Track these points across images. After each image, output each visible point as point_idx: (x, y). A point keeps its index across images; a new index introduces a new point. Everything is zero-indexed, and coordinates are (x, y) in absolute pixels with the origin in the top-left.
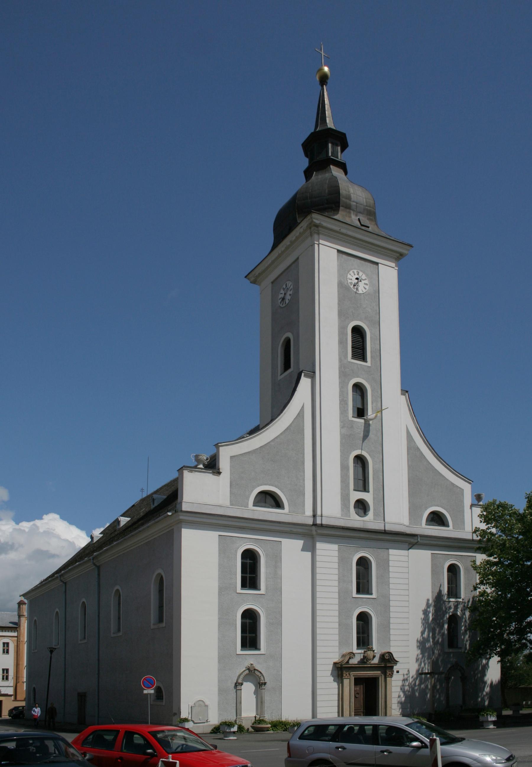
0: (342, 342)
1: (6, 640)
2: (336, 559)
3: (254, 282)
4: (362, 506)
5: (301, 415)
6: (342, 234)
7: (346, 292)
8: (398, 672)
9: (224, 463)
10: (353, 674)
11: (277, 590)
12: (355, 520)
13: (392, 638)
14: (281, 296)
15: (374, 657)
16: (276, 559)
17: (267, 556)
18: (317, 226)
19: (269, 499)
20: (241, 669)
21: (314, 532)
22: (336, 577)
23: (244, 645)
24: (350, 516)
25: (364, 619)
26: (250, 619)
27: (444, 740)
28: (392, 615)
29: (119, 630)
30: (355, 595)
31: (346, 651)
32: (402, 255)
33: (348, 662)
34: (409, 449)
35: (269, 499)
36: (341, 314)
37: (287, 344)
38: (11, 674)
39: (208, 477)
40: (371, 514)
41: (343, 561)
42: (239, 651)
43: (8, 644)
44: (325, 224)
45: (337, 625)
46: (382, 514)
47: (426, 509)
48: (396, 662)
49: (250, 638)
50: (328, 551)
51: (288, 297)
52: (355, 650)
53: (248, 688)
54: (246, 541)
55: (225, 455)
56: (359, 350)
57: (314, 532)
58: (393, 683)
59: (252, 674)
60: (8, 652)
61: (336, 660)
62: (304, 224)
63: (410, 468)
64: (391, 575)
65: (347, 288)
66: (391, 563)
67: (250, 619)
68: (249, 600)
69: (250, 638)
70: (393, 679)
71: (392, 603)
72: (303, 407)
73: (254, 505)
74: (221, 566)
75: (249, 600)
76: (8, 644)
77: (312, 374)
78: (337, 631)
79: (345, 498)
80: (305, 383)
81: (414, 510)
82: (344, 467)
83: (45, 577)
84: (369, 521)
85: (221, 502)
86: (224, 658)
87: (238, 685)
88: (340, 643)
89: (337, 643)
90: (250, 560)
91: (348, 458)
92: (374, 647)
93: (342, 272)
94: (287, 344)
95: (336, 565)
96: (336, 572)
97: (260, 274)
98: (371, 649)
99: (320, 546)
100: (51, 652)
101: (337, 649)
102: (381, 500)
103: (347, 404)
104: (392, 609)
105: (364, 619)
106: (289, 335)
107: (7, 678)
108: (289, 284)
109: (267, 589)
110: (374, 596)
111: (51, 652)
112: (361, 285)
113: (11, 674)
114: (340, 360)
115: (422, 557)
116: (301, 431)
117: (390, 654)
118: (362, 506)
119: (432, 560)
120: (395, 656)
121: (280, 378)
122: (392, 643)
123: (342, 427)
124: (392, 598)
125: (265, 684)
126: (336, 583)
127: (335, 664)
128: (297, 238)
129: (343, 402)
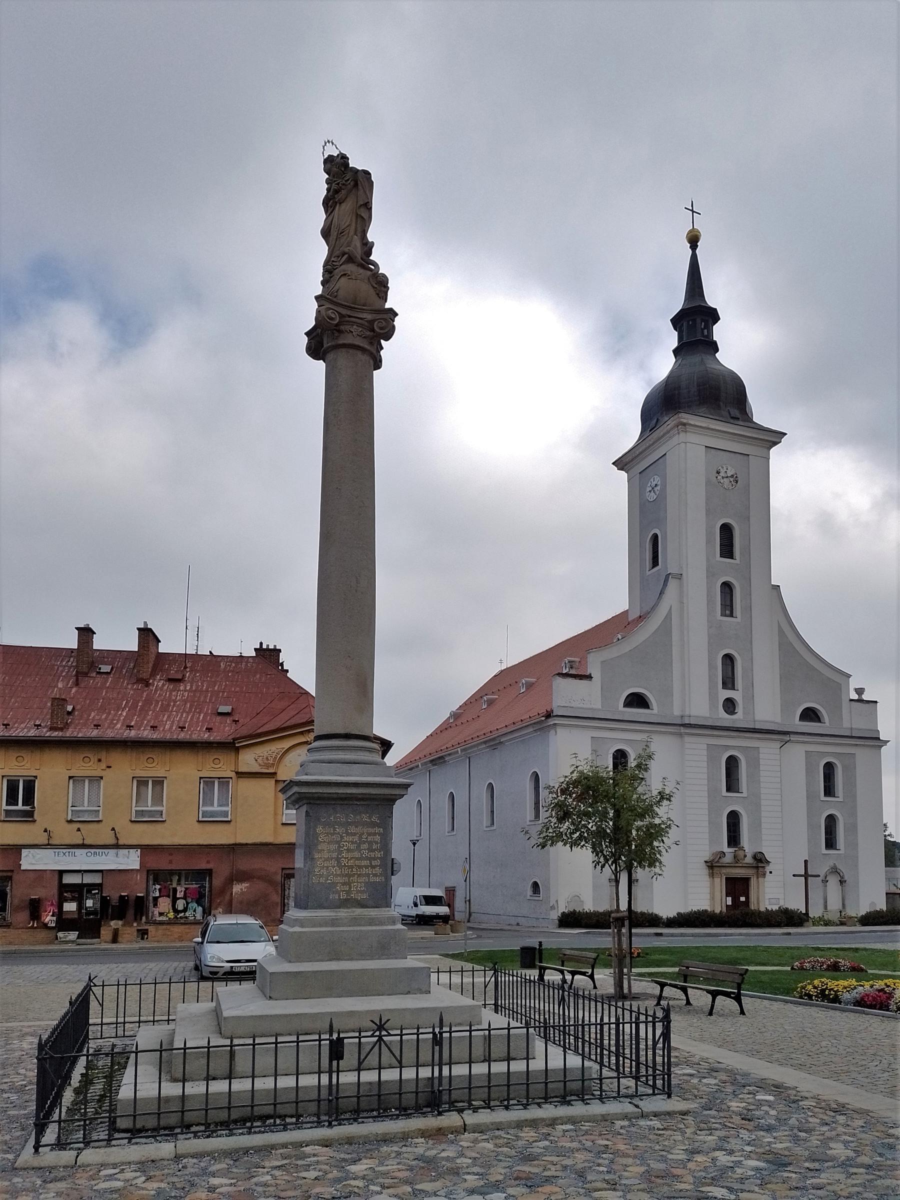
0: (709, 541)
2: (705, 758)
4: (730, 705)
5: (669, 616)
6: (712, 429)
8: (771, 872)
10: (724, 871)
12: (724, 718)
13: (764, 837)
15: (745, 856)
16: (755, 764)
18: (684, 424)
19: (637, 701)
22: (706, 776)
25: (734, 819)
26: (732, 784)
27: (90, 634)
28: (763, 814)
29: (493, 824)
33: (718, 862)
35: (637, 701)
36: (708, 512)
40: (740, 709)
41: (712, 760)
44: (692, 423)
47: (800, 705)
48: (768, 862)
50: (697, 748)
52: (726, 849)
54: (619, 739)
55: (593, 668)
58: (766, 884)
61: (707, 859)
66: (761, 762)
67: (732, 784)
71: (763, 803)
72: (695, 323)
77: (679, 577)
79: (713, 696)
81: (786, 707)
82: (712, 667)
84: (739, 718)
89: (707, 842)
92: (746, 848)
94: (655, 538)
95: (705, 764)
96: (705, 770)
98: (742, 849)
99: (687, 739)
100: (414, 844)
101: (707, 848)
102: (750, 698)
104: (763, 808)
105: (734, 819)
106: (657, 531)
110: (745, 795)
111: (414, 844)
114: (708, 560)
115: (797, 753)
118: (730, 705)
119: (806, 758)
121: (648, 573)
123: (710, 627)
125: (637, 880)
126: (706, 782)
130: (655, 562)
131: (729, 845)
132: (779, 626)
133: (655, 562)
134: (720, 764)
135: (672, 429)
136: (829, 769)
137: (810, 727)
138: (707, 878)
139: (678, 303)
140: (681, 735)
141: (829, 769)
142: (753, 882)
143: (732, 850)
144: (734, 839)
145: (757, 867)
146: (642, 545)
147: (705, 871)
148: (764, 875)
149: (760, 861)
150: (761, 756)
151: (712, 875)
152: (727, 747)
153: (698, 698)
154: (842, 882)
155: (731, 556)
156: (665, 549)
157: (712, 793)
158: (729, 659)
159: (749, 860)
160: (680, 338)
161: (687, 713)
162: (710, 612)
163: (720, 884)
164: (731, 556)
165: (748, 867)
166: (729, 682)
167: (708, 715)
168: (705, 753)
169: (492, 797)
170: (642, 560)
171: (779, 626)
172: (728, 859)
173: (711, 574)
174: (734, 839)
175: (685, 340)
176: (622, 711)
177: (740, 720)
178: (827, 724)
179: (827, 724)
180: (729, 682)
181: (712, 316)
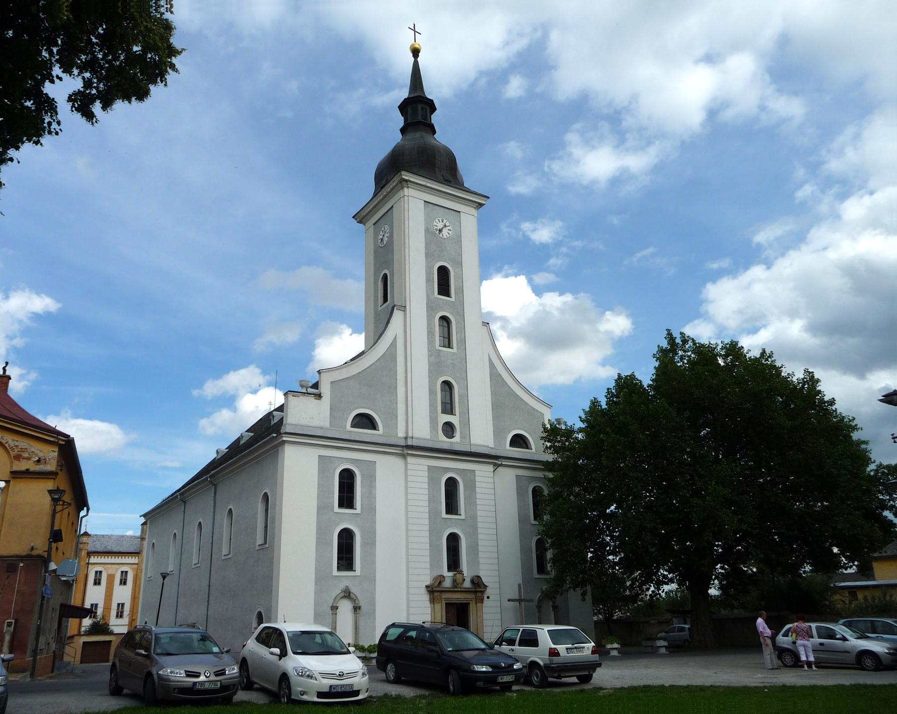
0: (429, 280)
1: (125, 568)
2: (426, 480)
3: (360, 222)
4: (449, 429)
7: (432, 236)
8: (488, 598)
9: (325, 389)
10: (445, 596)
11: (371, 509)
12: (443, 441)
14: (381, 237)
16: (371, 479)
17: (362, 476)
18: (407, 181)
19: (365, 421)
20: (338, 590)
21: (408, 449)
23: (341, 505)
24: (430, 468)
25: (453, 540)
26: (346, 539)
30: (444, 515)
31: (437, 573)
32: (481, 205)
34: (491, 375)
36: (428, 255)
37: (385, 277)
38: (127, 609)
39: (311, 400)
40: (458, 434)
41: (432, 481)
42: (335, 572)
43: (126, 572)
45: (428, 546)
46: (466, 435)
49: (346, 558)
50: (420, 466)
51: (386, 239)
53: (345, 607)
54: (346, 458)
56: (444, 287)
57: (408, 449)
58: (485, 610)
59: (347, 594)
60: (125, 583)
61: (428, 583)
62: (396, 180)
63: (494, 393)
64: (478, 496)
65: (433, 234)
67: (346, 539)
68: (345, 519)
69: (346, 558)
70: (484, 604)
73: (353, 426)
74: (320, 485)
75: (345, 519)
76: (126, 572)
77: (403, 308)
78: (428, 553)
79: (433, 420)
80: (397, 315)
81: (498, 432)
82: (432, 392)
83: (167, 496)
85: (321, 424)
86: (321, 579)
87: (334, 608)
88: (431, 565)
90: (347, 481)
91: (436, 384)
93: (429, 220)
94: (385, 277)
95: (426, 486)
96: (426, 492)
97: (364, 217)
98: (461, 572)
99: (410, 460)
100: (164, 577)
101: (428, 572)
102: (466, 423)
103: (434, 335)
105: (453, 540)
107: (121, 616)
108: (387, 227)
109: (362, 509)
110: (463, 517)
111: (164, 577)
112: (445, 231)
113: (127, 609)
114: (428, 297)
116: (394, 359)
117: (478, 577)
118: (449, 429)
120: (485, 580)
121: (380, 309)
122: (481, 567)
123: (430, 356)
124: (479, 519)
126: (427, 504)
127: (427, 587)
128: (392, 190)
129: (430, 333)
130: (385, 299)
131: (449, 569)
132: (490, 360)
133: (385, 299)
134: (334, 477)
135: (397, 185)
136: (451, 484)
137: (517, 452)
138: (428, 604)
139: (404, 94)
140: (404, 456)
141: (451, 484)
142: (472, 607)
143: (451, 574)
144: (454, 563)
145: (476, 592)
146: (376, 284)
147: (426, 597)
148: (482, 601)
149: (478, 585)
150: (477, 479)
151: (433, 601)
152: (447, 470)
153: (418, 419)
154: (356, 609)
155: (448, 294)
156: (393, 287)
157: (322, 509)
158: (447, 385)
159: (467, 584)
160: (405, 120)
161: (410, 435)
162: (431, 341)
163: (440, 608)
164: (448, 294)
165: (467, 591)
166: (448, 408)
167: (428, 437)
168: (426, 474)
169: (267, 510)
170: (376, 297)
171: (490, 360)
172: (447, 584)
173: (431, 308)
174: (454, 563)
175: (410, 121)
176: (348, 430)
177: (457, 443)
178: (534, 450)
179: (534, 450)
180: (448, 408)
181: (431, 106)
